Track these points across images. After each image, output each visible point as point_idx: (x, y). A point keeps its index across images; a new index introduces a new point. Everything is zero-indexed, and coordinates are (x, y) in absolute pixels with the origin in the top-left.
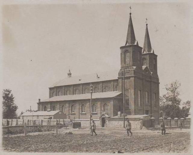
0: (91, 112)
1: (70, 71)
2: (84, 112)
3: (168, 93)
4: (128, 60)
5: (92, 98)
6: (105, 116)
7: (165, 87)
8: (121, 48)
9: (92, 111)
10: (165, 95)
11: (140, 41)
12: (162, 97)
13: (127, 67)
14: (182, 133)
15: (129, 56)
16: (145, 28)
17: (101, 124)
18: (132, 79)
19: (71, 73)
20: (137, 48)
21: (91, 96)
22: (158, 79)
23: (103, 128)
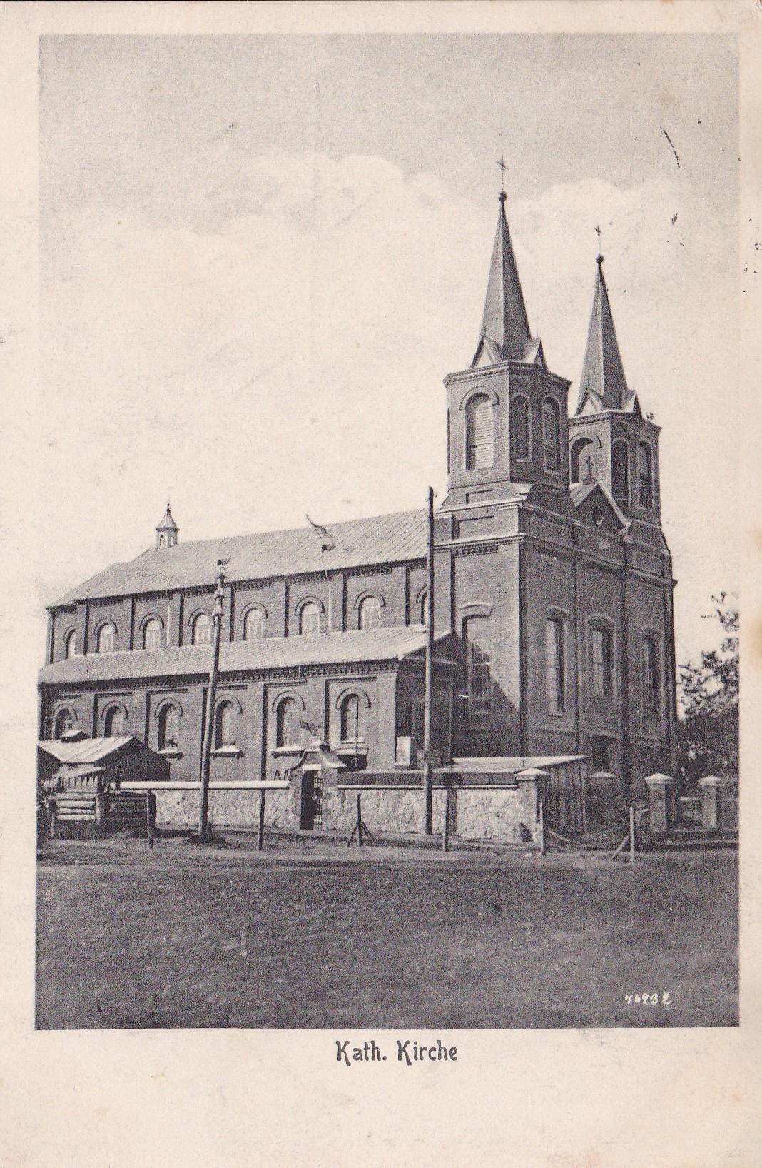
0: (209, 747)
1: (169, 511)
2: (234, 743)
3: (730, 640)
4: (485, 457)
5: (223, 667)
6: (320, 762)
7: (711, 607)
8: (451, 380)
9: (213, 746)
10: (712, 656)
11: (566, 352)
12: (698, 663)
13: (482, 489)
14: (345, 864)
15: (493, 423)
16: (594, 277)
17: (299, 809)
18: (512, 552)
19: (178, 526)
20: (534, 390)
21: (216, 662)
22: (666, 563)
23: (309, 832)
